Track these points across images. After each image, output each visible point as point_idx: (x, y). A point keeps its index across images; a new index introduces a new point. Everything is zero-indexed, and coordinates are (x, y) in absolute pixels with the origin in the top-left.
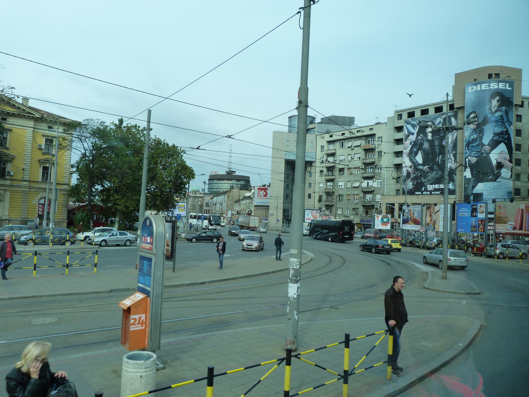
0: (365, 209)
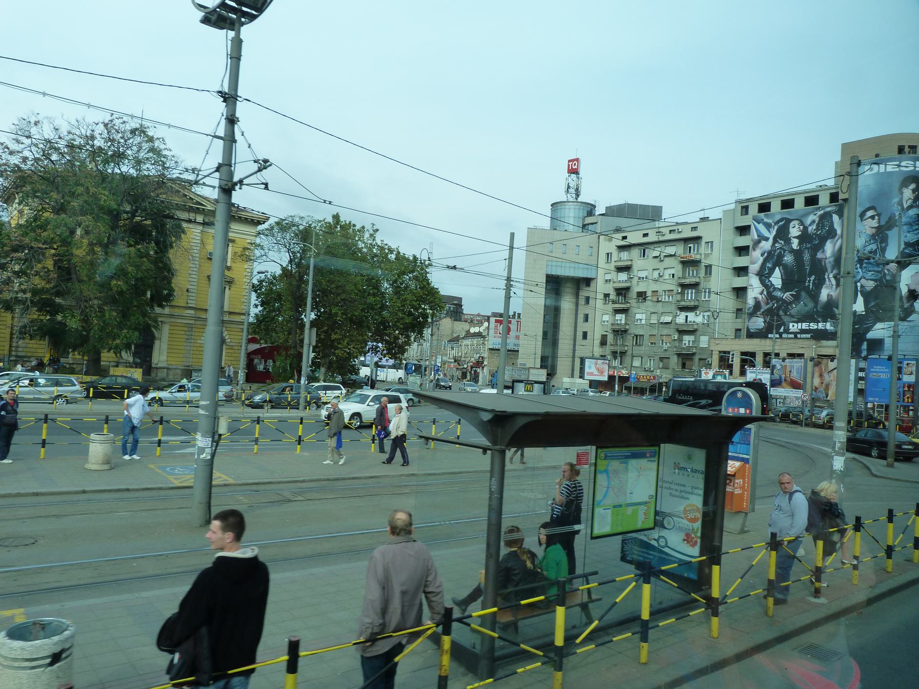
0: (680, 359)
